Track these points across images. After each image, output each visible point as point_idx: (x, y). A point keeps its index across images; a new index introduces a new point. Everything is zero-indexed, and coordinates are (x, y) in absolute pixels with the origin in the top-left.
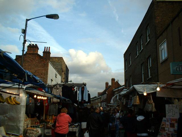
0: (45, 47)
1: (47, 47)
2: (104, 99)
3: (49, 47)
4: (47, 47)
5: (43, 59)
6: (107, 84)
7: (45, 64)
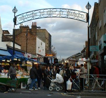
0: (33, 22)
1: (34, 22)
3: (36, 22)
4: (34, 22)
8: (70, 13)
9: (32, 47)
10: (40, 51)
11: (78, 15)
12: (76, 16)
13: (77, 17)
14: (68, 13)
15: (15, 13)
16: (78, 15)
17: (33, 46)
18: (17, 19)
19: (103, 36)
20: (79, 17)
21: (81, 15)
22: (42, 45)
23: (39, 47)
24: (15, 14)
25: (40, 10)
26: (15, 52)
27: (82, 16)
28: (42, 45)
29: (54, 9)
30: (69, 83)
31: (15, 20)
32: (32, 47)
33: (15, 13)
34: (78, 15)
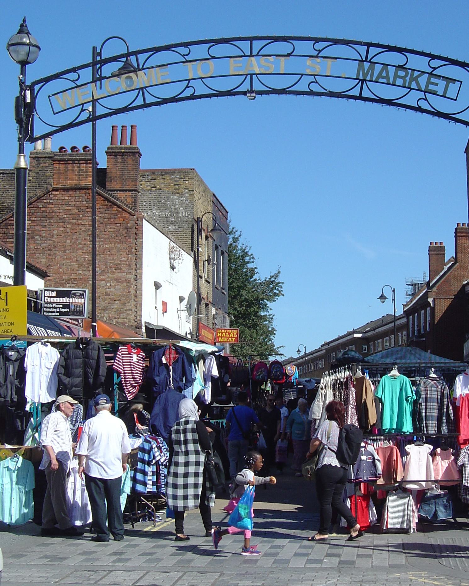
2: (419, 331)
5: (119, 207)
6: (436, 251)
7: (127, 228)
8: (378, 68)
9: (118, 280)
10: (165, 304)
11: (423, 80)
12: (414, 85)
13: (422, 95)
14: (360, 67)
15: (24, 64)
16: (429, 83)
17: (119, 274)
18: (41, 105)
19: (436, 321)
20: (435, 93)
21: (442, 84)
22: (173, 268)
23: (157, 286)
24: (23, 72)
25: (186, 45)
26: (98, 83)
27: (453, 89)
28: (173, 268)
29: (276, 39)
30: (397, 484)
31: (25, 112)
32: (118, 280)
33: (24, 64)
34: (423, 80)
